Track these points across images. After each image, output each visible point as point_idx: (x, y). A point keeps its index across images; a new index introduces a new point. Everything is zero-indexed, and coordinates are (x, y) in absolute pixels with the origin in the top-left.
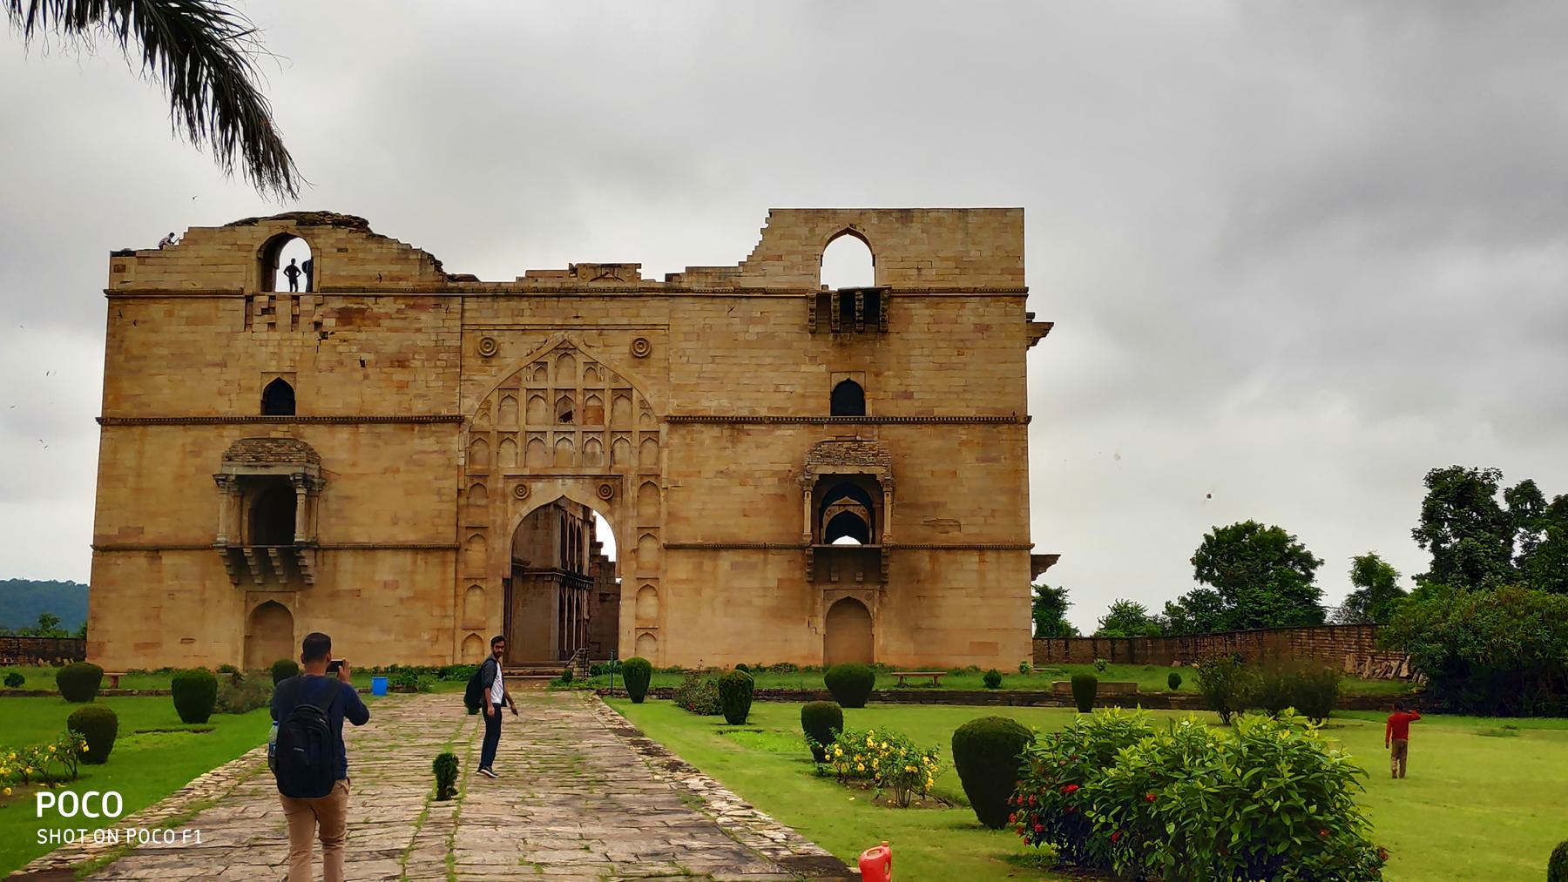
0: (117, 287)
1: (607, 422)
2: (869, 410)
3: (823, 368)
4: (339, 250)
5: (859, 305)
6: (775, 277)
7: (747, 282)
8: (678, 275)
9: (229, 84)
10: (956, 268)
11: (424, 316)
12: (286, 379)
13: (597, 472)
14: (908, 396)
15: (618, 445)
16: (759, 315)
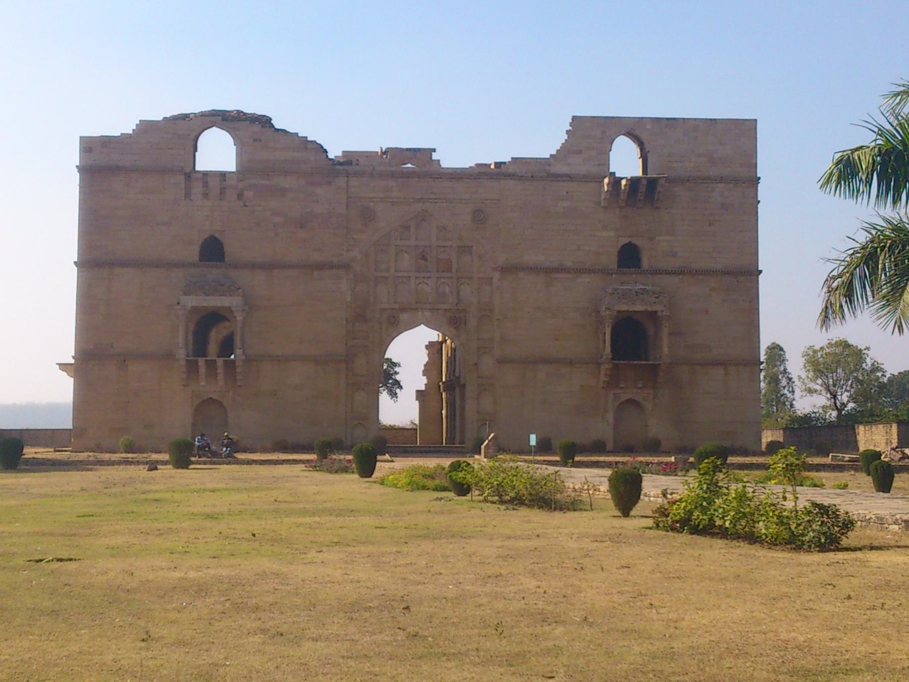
0: (194, 176)
1: (454, 270)
2: (645, 263)
3: (611, 234)
4: (255, 140)
5: (642, 189)
6: (577, 165)
7: (560, 168)
8: (505, 163)
9: (844, 174)
10: (708, 162)
11: (318, 190)
12: (217, 235)
13: (446, 307)
14: (674, 255)
15: (462, 287)
16: (565, 194)
